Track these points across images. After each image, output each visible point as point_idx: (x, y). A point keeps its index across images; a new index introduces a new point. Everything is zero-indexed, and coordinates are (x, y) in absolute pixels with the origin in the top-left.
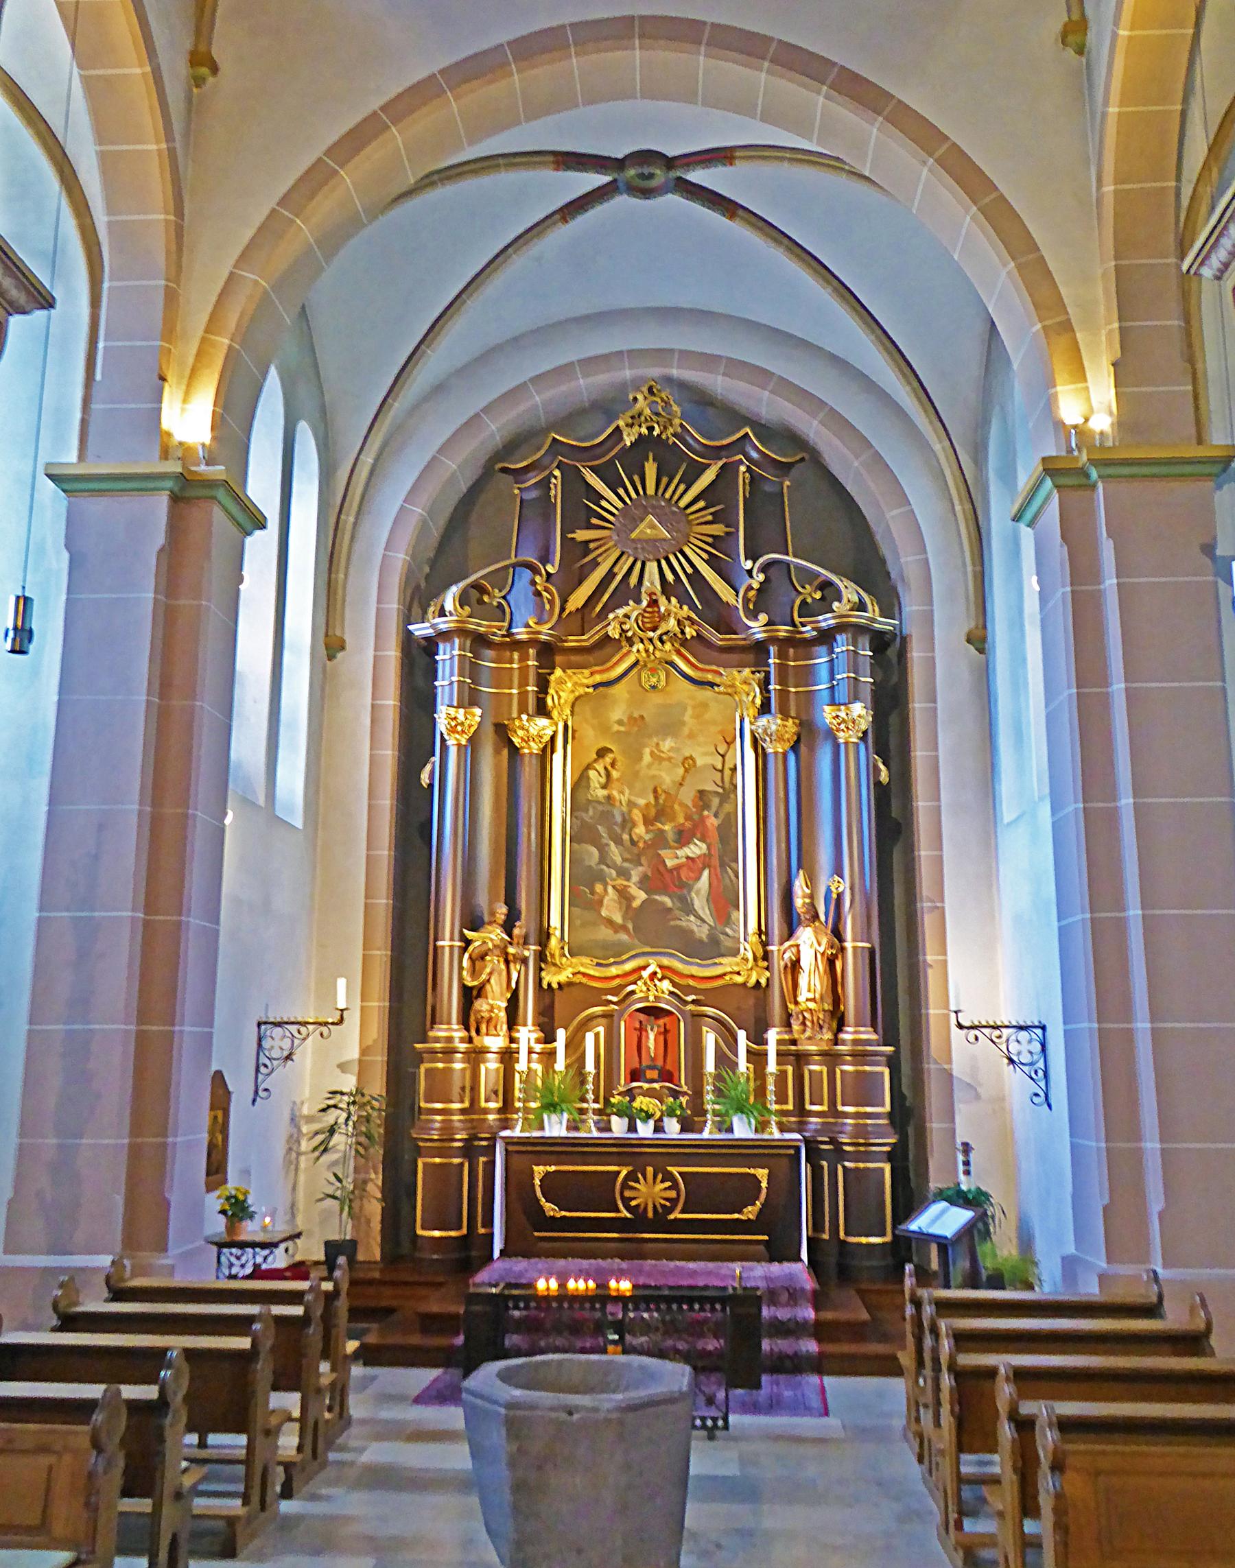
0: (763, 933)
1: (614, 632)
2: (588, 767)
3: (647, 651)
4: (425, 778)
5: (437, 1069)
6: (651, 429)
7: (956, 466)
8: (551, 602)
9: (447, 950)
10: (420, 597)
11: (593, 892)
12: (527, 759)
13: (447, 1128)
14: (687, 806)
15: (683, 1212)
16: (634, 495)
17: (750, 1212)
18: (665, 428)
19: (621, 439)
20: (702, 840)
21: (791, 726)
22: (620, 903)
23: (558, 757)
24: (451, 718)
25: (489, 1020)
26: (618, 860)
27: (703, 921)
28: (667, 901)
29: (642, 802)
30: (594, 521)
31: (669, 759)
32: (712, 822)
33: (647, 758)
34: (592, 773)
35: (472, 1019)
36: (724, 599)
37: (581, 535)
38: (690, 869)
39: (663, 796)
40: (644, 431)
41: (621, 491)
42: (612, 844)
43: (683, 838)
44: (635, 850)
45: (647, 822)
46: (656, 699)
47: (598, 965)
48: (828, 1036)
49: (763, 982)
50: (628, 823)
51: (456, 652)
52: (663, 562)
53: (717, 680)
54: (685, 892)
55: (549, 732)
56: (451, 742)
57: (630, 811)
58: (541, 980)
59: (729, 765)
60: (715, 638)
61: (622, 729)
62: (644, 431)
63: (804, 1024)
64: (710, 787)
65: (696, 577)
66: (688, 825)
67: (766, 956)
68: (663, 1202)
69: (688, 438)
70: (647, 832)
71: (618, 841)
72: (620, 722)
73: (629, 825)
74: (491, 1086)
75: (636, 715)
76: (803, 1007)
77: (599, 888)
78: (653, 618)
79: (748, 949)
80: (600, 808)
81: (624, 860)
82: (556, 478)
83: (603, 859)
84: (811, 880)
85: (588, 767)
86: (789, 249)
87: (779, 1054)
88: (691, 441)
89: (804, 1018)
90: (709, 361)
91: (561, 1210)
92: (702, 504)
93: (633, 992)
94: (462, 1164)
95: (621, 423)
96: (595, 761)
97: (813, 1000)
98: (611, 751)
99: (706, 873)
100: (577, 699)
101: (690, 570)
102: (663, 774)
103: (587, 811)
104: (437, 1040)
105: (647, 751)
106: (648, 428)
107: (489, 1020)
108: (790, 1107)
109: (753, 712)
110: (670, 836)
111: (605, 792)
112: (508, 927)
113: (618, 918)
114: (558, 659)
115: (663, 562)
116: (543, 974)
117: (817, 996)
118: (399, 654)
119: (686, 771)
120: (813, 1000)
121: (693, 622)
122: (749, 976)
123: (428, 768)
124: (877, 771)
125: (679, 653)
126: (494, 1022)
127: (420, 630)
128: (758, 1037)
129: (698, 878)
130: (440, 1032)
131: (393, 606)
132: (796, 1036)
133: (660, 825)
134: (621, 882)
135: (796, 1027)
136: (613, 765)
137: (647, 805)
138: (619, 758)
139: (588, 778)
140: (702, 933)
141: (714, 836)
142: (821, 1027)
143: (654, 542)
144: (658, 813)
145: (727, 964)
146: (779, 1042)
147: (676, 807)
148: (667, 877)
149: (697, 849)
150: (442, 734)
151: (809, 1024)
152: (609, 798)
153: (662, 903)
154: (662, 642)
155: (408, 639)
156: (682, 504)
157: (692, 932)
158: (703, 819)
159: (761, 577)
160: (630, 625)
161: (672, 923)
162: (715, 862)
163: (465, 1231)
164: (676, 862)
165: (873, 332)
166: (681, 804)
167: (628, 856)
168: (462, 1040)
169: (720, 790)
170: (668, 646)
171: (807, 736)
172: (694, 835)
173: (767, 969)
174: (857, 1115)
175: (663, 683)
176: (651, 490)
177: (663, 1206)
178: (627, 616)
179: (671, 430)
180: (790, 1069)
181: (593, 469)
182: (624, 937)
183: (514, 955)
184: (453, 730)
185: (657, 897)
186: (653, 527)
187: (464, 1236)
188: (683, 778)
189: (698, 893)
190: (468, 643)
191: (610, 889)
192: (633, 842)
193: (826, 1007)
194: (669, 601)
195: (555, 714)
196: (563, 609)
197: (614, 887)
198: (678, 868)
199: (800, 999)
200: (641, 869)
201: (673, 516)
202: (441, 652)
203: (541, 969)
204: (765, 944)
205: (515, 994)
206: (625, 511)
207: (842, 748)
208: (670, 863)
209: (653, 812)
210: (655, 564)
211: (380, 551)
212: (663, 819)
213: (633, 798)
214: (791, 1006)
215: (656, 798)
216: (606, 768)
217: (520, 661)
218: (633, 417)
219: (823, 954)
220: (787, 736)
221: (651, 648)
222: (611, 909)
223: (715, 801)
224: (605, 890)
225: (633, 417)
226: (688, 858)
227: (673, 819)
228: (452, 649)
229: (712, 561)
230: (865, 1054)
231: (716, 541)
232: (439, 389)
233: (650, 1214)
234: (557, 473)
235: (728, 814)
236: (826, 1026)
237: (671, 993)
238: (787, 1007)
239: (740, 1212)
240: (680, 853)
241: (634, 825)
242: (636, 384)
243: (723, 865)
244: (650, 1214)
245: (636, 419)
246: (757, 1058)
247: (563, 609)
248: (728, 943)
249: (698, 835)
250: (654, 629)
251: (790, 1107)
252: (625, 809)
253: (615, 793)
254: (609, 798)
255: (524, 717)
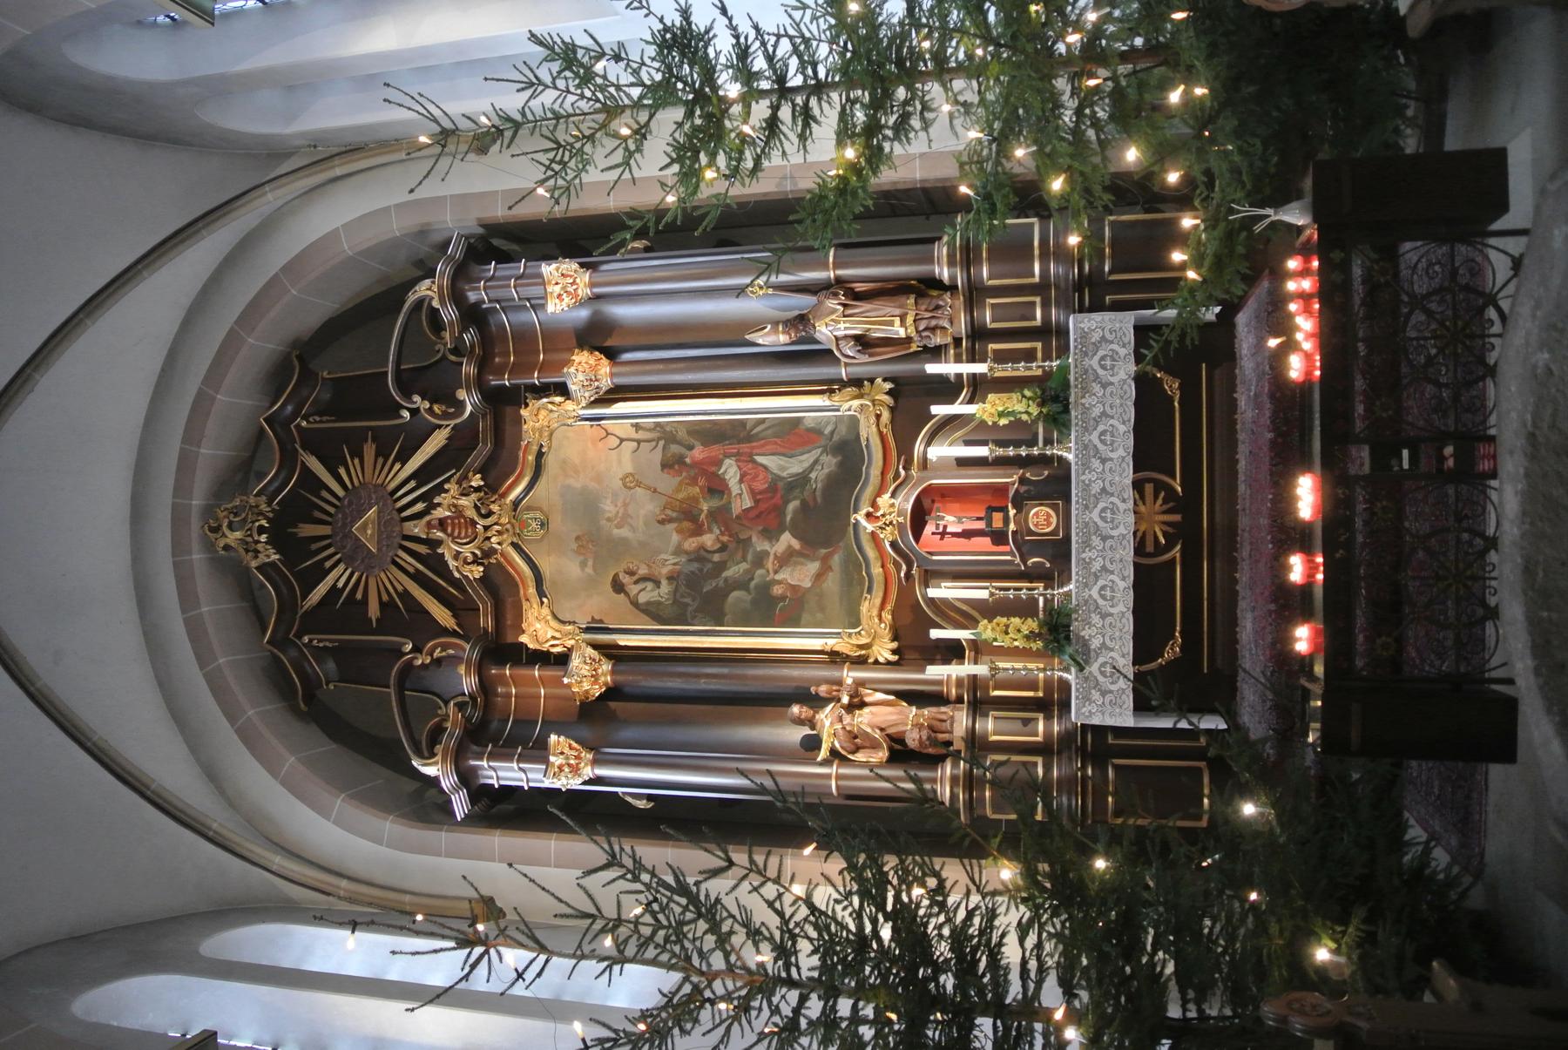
0: (830, 387)
1: (477, 572)
2: (635, 604)
3: (500, 533)
4: (642, 804)
5: (992, 797)
6: (261, 530)
7: (291, 177)
8: (445, 647)
9: (841, 783)
10: (426, 806)
11: (783, 598)
12: (620, 678)
13: (1067, 784)
14: (681, 483)
15: (1174, 478)
16: (331, 550)
17: (1172, 386)
18: (261, 513)
19: (273, 564)
20: (719, 463)
21: (582, 358)
22: (796, 564)
23: (624, 640)
24: (565, 768)
25: (932, 728)
26: (744, 566)
27: (816, 462)
28: (793, 506)
29: (675, 538)
30: (359, 596)
31: (625, 505)
32: (699, 453)
33: (624, 532)
34: (643, 598)
35: (931, 750)
36: (444, 442)
37: (374, 611)
38: (754, 478)
39: (669, 512)
40: (263, 538)
41: (328, 564)
42: (725, 574)
43: (717, 488)
44: (732, 546)
45: (698, 531)
46: (556, 522)
47: (870, 591)
48: (947, 296)
49: (888, 386)
50: (700, 556)
51: (484, 763)
52: (404, 514)
53: (535, 448)
54: (780, 484)
55: (590, 651)
56: (588, 772)
57: (687, 553)
58: (889, 663)
59: (632, 433)
60: (490, 449)
61: (590, 563)
62: (263, 538)
63: (933, 329)
64: (657, 456)
65: (421, 475)
66: (702, 482)
67: (857, 382)
68: (1160, 501)
69: (272, 488)
70: (710, 531)
71: (722, 566)
72: (583, 565)
73: (703, 553)
74: (1018, 725)
75: (574, 546)
76: (912, 331)
77: (777, 590)
78: (457, 524)
79: (848, 405)
80: (683, 589)
81: (744, 559)
82: (311, 641)
83: (742, 584)
84: (757, 325)
85: (635, 604)
86: (36, 369)
87: (972, 360)
88: (276, 484)
89: (926, 329)
90: (186, 465)
91: (1173, 637)
92: (342, 471)
93: (893, 544)
94: (1116, 767)
95: (254, 564)
96: (627, 594)
97: (903, 318)
98: (616, 575)
99: (760, 459)
100: (555, 617)
101: (412, 484)
102: (642, 512)
103: (687, 605)
104: (953, 796)
105: (616, 531)
106: (260, 534)
107: (932, 728)
108: (1039, 345)
109: (569, 405)
110: (715, 503)
111: (664, 582)
112: (817, 702)
113: (814, 567)
114: (510, 639)
115: (404, 514)
116: (881, 660)
117: (898, 312)
118: (498, 832)
119: (639, 484)
120: (903, 318)
121: (465, 477)
122: (882, 403)
123: (629, 799)
124: (634, 250)
125: (504, 495)
126: (936, 723)
127: (460, 805)
128: (947, 389)
129: (765, 467)
130: (945, 792)
131: (443, 837)
132: (949, 340)
133: (703, 516)
134: (770, 564)
135: (938, 340)
136: (631, 573)
137: (679, 531)
138: (624, 566)
139: (648, 603)
140: (830, 463)
141: (716, 450)
142: (938, 307)
143: (383, 525)
144: (688, 517)
145: (868, 431)
146: (958, 360)
147: (680, 496)
148: (763, 506)
149: (730, 471)
150: (585, 783)
151: (933, 323)
152: (670, 578)
153: (795, 512)
154: (490, 514)
155: (470, 820)
156: (341, 493)
157: (829, 476)
158: (695, 464)
159: (417, 398)
160: (467, 551)
161: (819, 500)
162: (745, 448)
163: (1202, 764)
164: (745, 496)
165: (140, 272)
166: (678, 490)
167: (740, 554)
168: (955, 765)
169: (662, 443)
170: (495, 508)
171: (597, 336)
172: (715, 475)
173: (872, 381)
174: (1044, 256)
175: (538, 515)
176: (326, 530)
177: (1165, 501)
178: (457, 556)
179: (264, 507)
180: (992, 346)
181: (304, 597)
182: (836, 560)
183: (851, 697)
184: (575, 770)
185: (788, 518)
186: (364, 527)
187: (1210, 766)
188: (649, 488)
189: (783, 468)
190: (475, 748)
191: (778, 577)
192: (723, 548)
193: (911, 301)
194: (439, 505)
195: (570, 643)
196: (454, 634)
197: (776, 572)
198: (753, 493)
199: (902, 333)
200: (754, 539)
201: (355, 502)
202: (490, 781)
203: (876, 662)
204: (844, 384)
205: (901, 695)
206: (349, 560)
207: (596, 290)
208: (748, 503)
209: (686, 524)
210: (407, 524)
211: (383, 849)
212: (695, 512)
213: (671, 549)
214: (914, 348)
215: (670, 520)
216: (636, 582)
217: (507, 685)
218: (247, 551)
219: (845, 306)
220: (592, 362)
221: (497, 527)
222: (801, 575)
223: (675, 448)
224: (779, 582)
225: (247, 551)
226: (741, 481)
227: (695, 500)
228: (482, 768)
229: (403, 458)
230: (966, 248)
231: (382, 453)
232: (212, 775)
233: (1177, 518)
234: (306, 639)
235: (689, 433)
236: (935, 303)
237: (893, 495)
238: (916, 353)
239: (1171, 399)
240: (735, 489)
241: (702, 547)
242: (209, 546)
243: (749, 438)
244: (1177, 518)
245: (251, 548)
246: (978, 388)
247: (454, 634)
248: (843, 429)
249: (713, 469)
250: (474, 523)
251: (1039, 345)
252: (684, 559)
253: (665, 571)
254: (670, 578)
255: (566, 680)
